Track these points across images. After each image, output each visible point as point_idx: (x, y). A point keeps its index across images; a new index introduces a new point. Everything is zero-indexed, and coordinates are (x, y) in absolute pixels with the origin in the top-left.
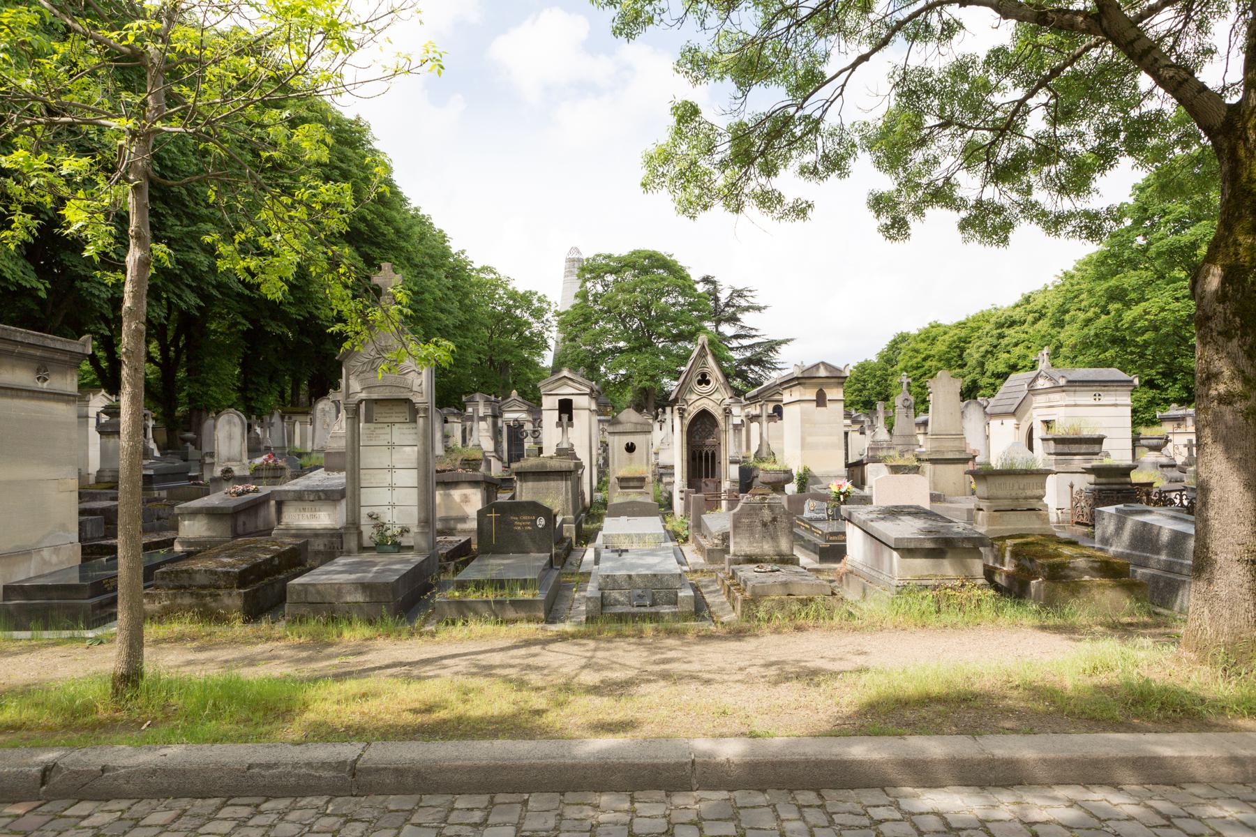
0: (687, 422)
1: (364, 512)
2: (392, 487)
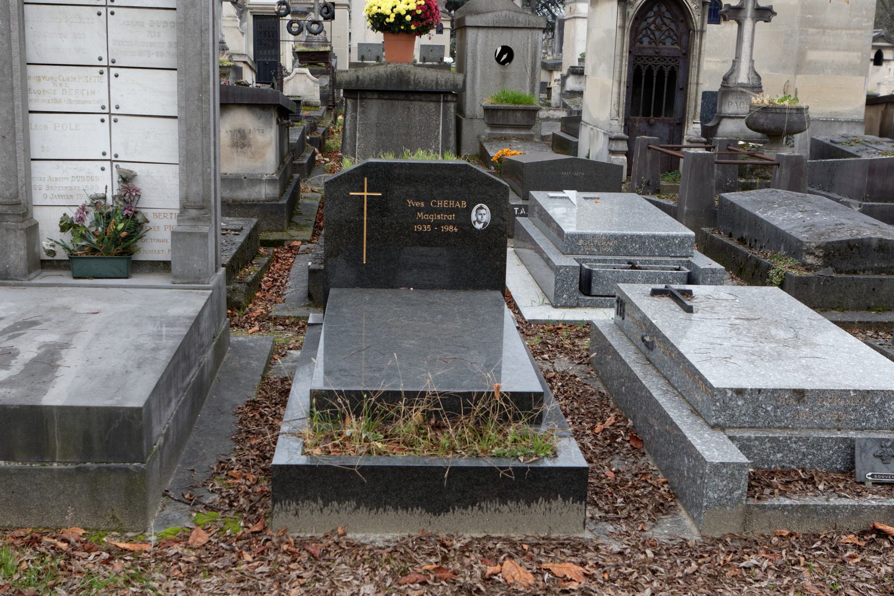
0: (632, 11)
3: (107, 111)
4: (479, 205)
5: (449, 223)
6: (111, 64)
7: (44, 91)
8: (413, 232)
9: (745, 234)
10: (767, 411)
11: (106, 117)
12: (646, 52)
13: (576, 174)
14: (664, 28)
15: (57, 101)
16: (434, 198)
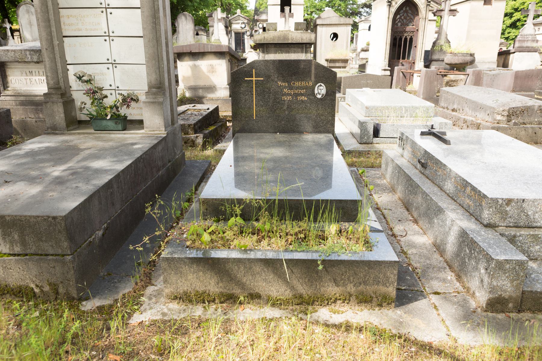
0: (393, 10)
1: (72, 70)
2: (108, 36)
3: (107, 34)
4: (319, 84)
5: (302, 95)
6: (107, 6)
7: (72, 24)
8: (281, 100)
9: (455, 107)
10: (528, 215)
11: (107, 38)
12: (399, 30)
13: (368, 82)
14: (408, 18)
15: (80, 30)
16: (293, 81)
